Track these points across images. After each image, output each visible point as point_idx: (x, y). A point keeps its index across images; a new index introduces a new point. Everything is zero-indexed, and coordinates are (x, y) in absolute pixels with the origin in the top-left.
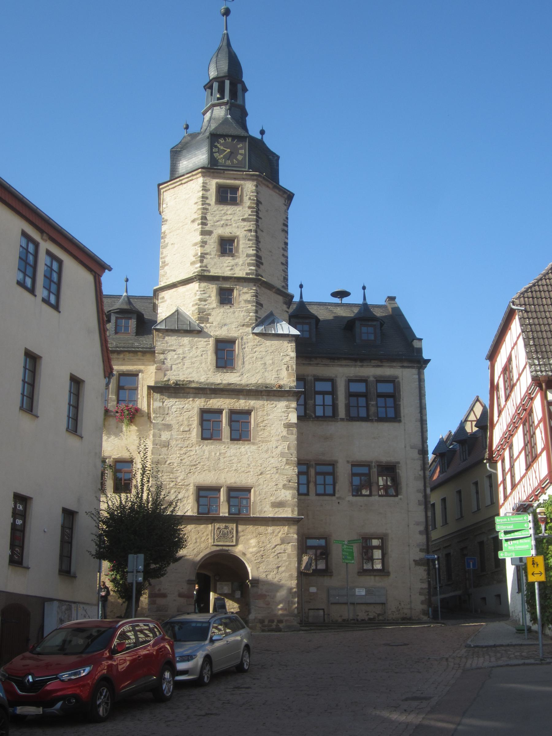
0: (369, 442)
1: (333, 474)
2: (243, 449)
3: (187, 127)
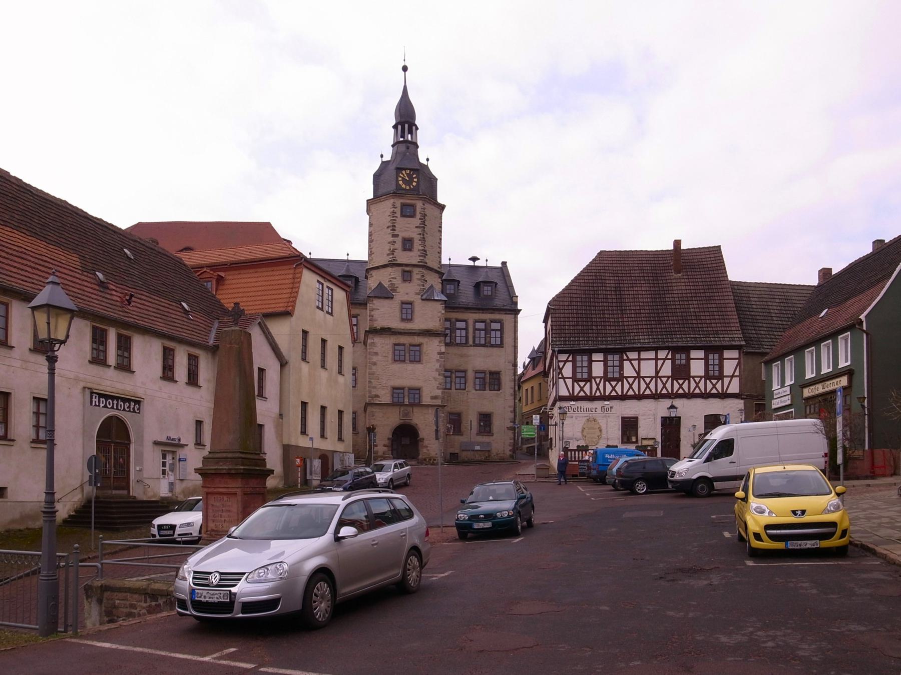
0: (479, 359)
1: (465, 377)
3: (382, 156)
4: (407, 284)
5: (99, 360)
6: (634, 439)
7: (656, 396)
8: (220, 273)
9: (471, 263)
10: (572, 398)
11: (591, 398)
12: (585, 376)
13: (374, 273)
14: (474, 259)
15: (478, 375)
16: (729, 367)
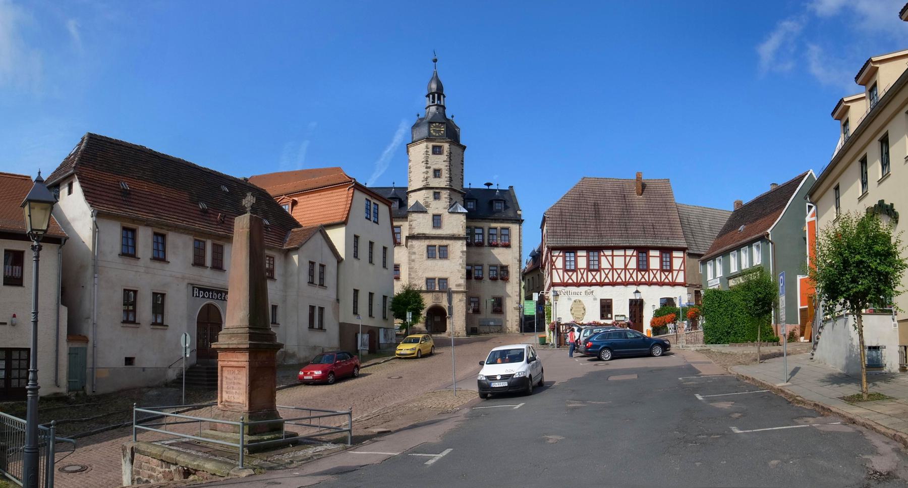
1: (482, 270)
2: (444, 263)
4: (437, 201)
5: (199, 262)
6: (609, 316)
7: (626, 284)
8: (296, 199)
9: (486, 187)
10: (566, 285)
11: (578, 285)
12: (573, 267)
13: (412, 194)
14: (489, 184)
15: (492, 268)
16: (677, 263)
